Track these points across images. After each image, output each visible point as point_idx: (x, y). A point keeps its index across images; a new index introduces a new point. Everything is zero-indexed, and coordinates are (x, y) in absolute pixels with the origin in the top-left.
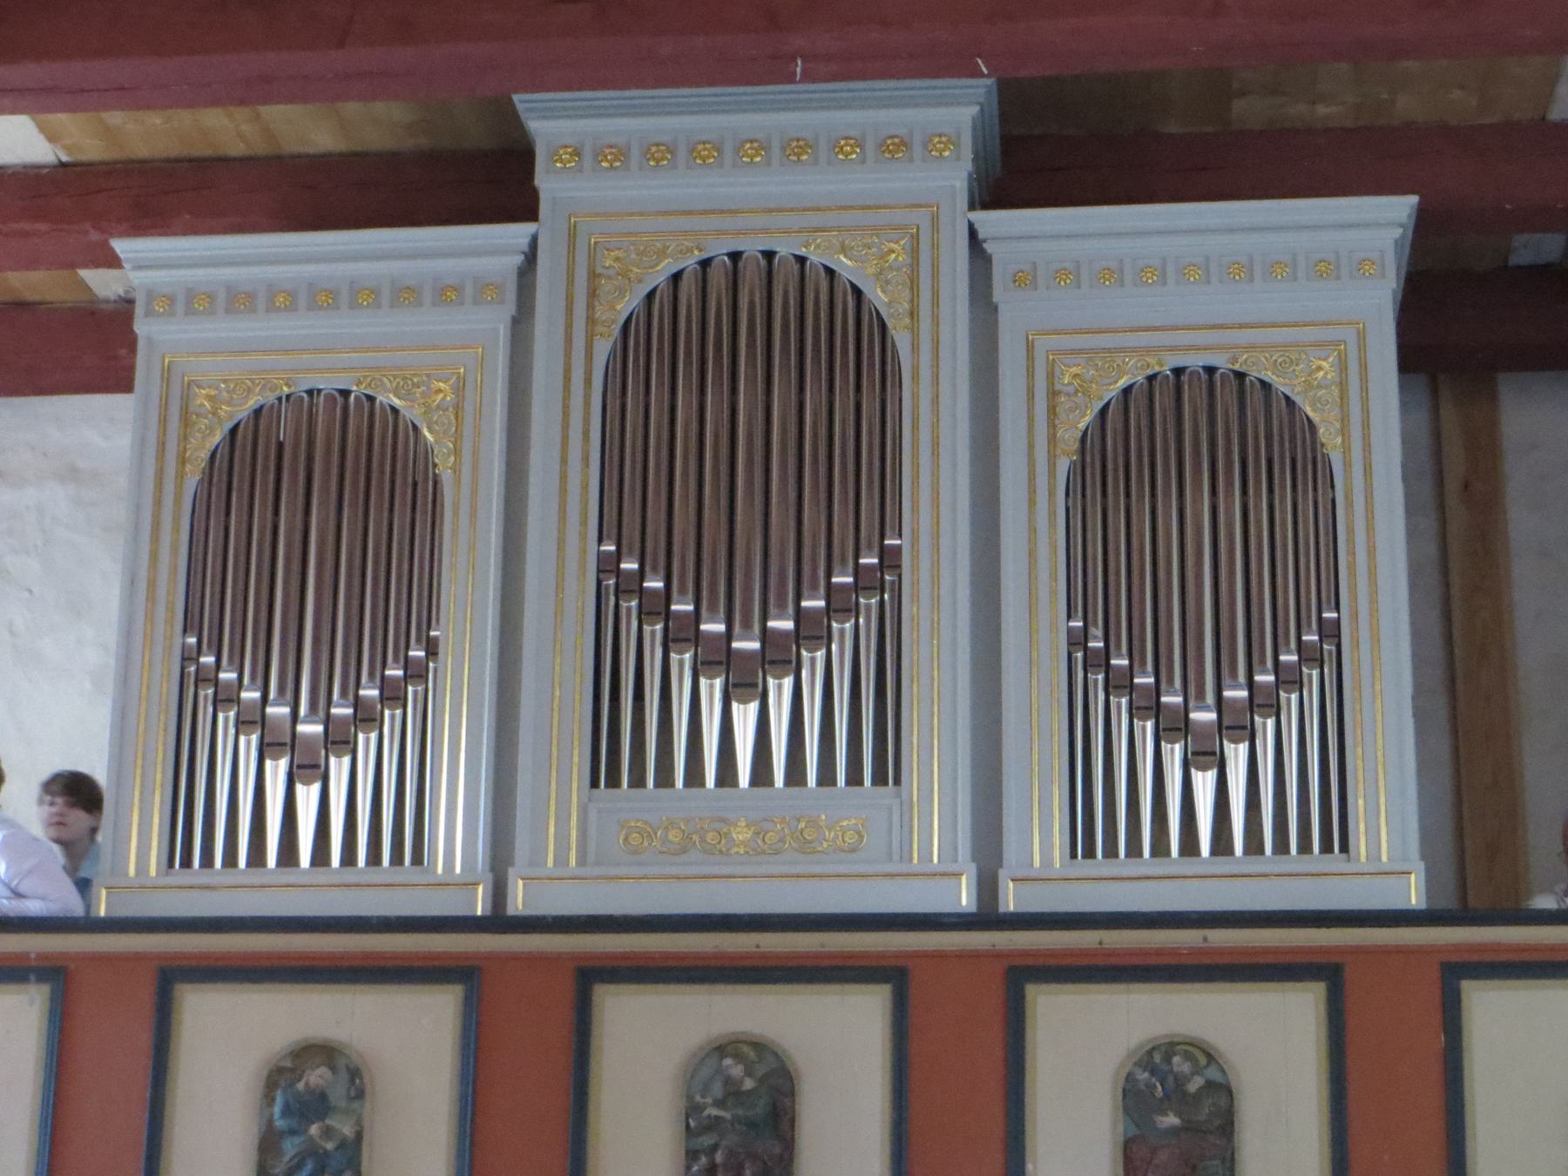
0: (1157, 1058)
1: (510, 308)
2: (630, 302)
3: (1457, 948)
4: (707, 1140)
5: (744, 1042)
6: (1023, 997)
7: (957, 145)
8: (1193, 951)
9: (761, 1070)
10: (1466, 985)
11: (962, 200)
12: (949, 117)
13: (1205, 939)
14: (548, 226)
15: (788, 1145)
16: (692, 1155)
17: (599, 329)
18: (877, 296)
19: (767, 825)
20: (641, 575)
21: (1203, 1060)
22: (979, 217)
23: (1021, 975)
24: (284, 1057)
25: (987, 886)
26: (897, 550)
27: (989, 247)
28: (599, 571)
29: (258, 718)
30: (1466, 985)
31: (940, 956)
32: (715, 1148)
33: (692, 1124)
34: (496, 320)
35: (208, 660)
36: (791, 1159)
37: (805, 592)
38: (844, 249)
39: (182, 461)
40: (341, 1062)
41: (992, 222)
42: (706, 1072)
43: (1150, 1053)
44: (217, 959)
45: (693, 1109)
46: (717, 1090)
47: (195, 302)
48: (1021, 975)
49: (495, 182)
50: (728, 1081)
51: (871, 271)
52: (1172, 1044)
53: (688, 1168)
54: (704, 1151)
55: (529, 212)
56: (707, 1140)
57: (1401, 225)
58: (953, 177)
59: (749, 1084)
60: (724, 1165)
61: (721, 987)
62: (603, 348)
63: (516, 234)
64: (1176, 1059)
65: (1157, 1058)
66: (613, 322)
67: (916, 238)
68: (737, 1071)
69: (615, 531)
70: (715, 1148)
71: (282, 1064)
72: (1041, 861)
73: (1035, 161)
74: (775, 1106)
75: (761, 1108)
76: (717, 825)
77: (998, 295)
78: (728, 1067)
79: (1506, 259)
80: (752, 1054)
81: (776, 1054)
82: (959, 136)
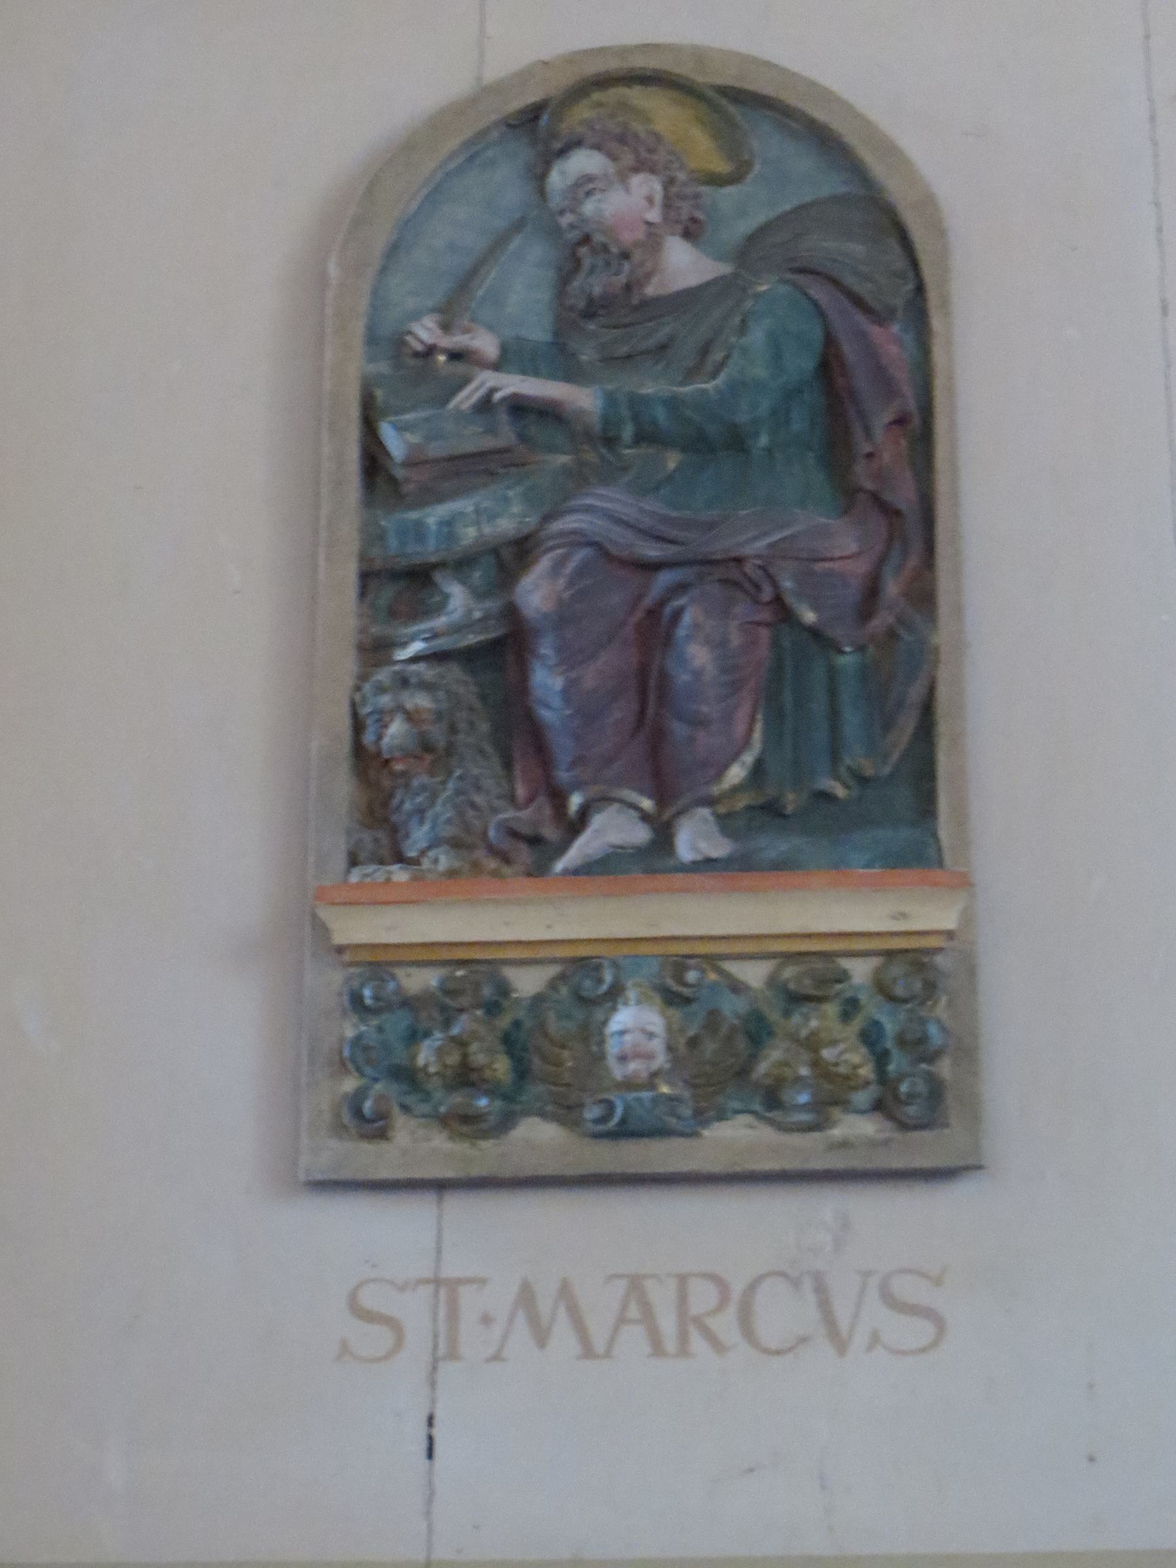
4: (478, 516)
9: (743, 210)
15: (909, 526)
16: (398, 584)
32: (516, 555)
33: (395, 443)
36: (924, 597)
42: (460, 227)
45: (405, 371)
46: (524, 293)
50: (578, 249)
53: (374, 651)
54: (462, 565)
56: (478, 516)
59: (683, 265)
60: (564, 617)
68: (628, 203)
70: (516, 555)
74: (829, 365)
75: (759, 358)
78: (585, 186)
79: (590, 294)
80: (703, 151)
81: (825, 142)
82: (870, 1348)
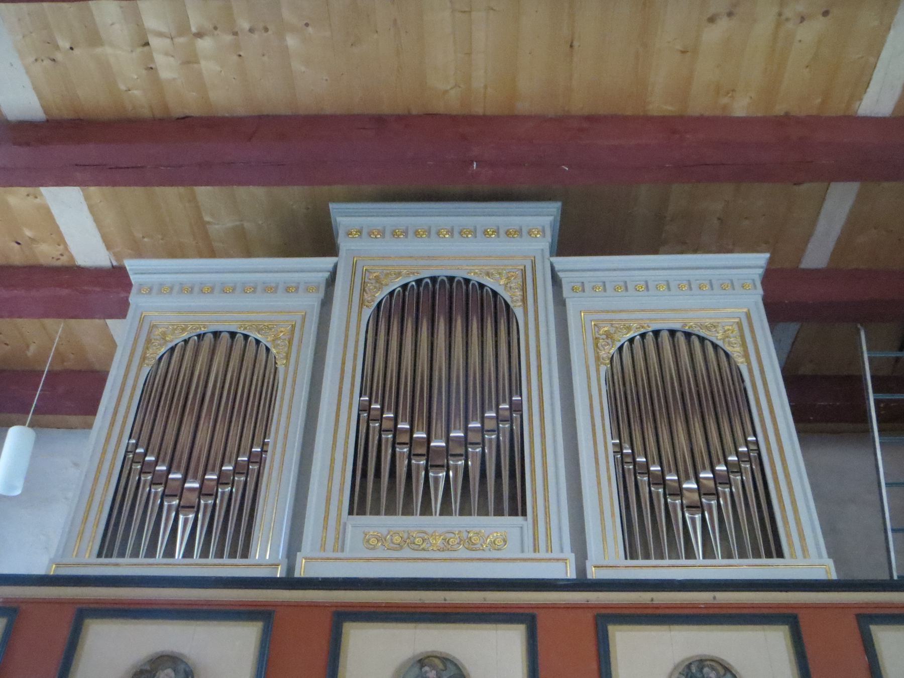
0: (694, 669)
1: (321, 294)
2: (381, 295)
3: (867, 605)
5: (436, 657)
6: (607, 631)
7: (544, 231)
8: (708, 606)
10: (611, 628)
11: (547, 253)
12: (539, 220)
13: (714, 598)
14: (343, 261)
17: (147, 361)
18: (505, 294)
19: (449, 536)
20: (382, 411)
21: (722, 671)
22: (555, 260)
23: (605, 619)
24: (145, 664)
25: (581, 569)
26: (520, 403)
27: (561, 275)
28: (359, 410)
29: (163, 481)
30: (611, 628)
31: (554, 607)
34: (313, 301)
35: (140, 450)
37: (241, 454)
38: (488, 274)
39: (144, 358)
40: (181, 667)
41: (562, 262)
43: (689, 666)
44: (130, 604)
47: (164, 290)
48: (605, 619)
49: (321, 240)
51: (502, 282)
52: (701, 661)
55: (337, 255)
57: (762, 267)
58: (542, 244)
61: (422, 625)
62: (368, 312)
63: (327, 262)
64: (706, 670)
65: (694, 669)
66: (373, 301)
67: (293, 327)
69: (137, 436)
71: (144, 668)
72: (608, 557)
73: (571, 241)
76: (422, 535)
77: (565, 294)
78: (426, 672)
80: (441, 666)
81: (456, 665)
